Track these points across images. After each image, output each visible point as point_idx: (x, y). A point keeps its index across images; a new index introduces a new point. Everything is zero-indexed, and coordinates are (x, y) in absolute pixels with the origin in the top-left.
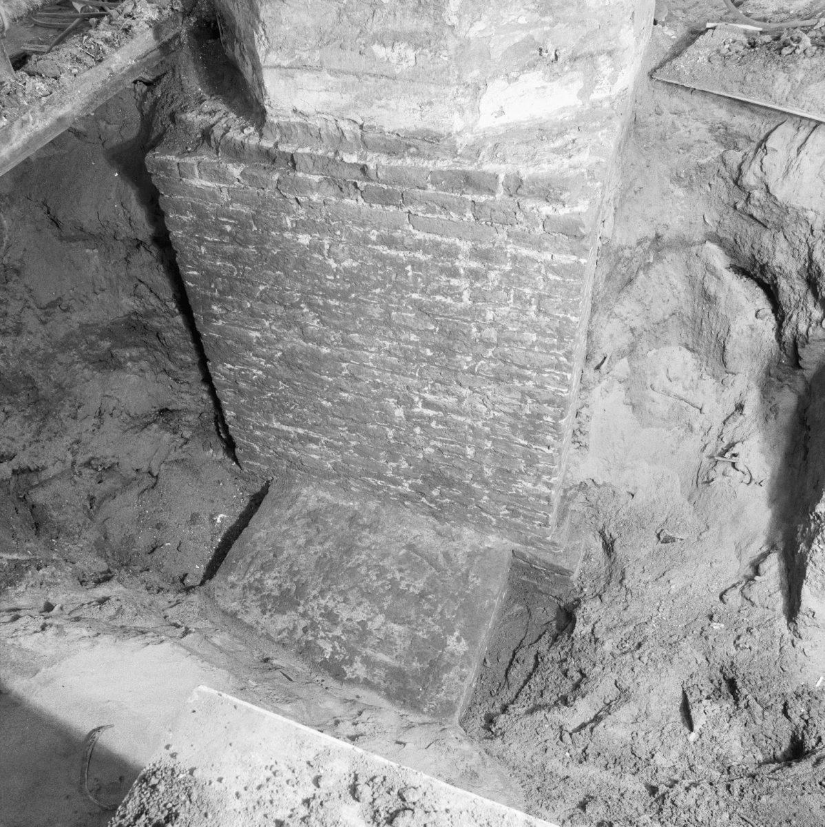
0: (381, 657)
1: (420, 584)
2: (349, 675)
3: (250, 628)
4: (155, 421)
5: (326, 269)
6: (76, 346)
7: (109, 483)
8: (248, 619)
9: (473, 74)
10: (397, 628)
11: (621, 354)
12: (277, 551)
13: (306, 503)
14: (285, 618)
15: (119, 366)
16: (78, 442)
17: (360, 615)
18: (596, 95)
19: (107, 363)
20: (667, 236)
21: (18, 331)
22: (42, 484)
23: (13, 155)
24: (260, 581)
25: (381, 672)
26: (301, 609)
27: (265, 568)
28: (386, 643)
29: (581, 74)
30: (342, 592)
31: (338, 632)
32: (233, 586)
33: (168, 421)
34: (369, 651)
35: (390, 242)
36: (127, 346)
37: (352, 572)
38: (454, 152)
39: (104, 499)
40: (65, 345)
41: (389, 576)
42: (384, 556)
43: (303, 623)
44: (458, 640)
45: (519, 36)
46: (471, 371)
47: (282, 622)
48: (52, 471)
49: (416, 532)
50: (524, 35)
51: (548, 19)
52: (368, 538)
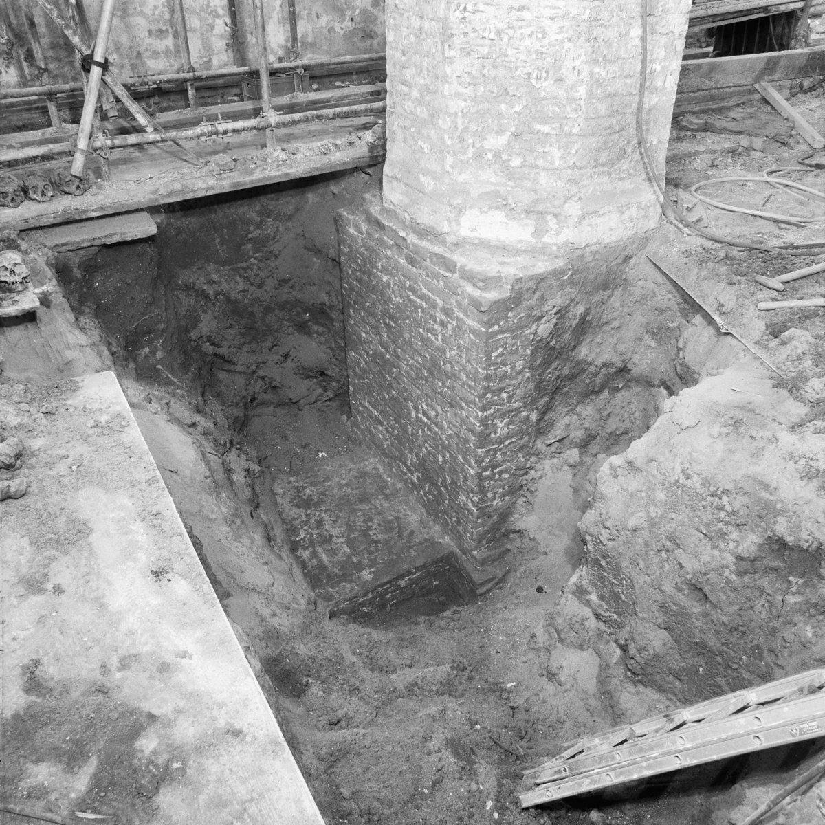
0: (324, 557)
1: (381, 537)
2: (298, 553)
3: (277, 504)
4: (316, 377)
5: (390, 299)
6: (289, 311)
7: (269, 396)
8: (279, 500)
9: (458, 201)
10: (346, 548)
11: (574, 445)
12: (327, 479)
13: (366, 466)
14: (298, 511)
15: (309, 334)
16: (264, 363)
17: (334, 532)
18: (546, 239)
19: (302, 328)
20: (635, 371)
21: (260, 286)
22: (229, 371)
23: (252, 182)
24: (304, 488)
25: (315, 562)
26: (309, 512)
27: (313, 484)
28: (333, 553)
29: (533, 222)
30: (338, 517)
31: (315, 532)
32: (290, 482)
33: (323, 381)
34: (320, 550)
35: (413, 291)
36: (317, 323)
37: (354, 511)
38: (444, 242)
39: (263, 403)
40: (283, 306)
41: (370, 524)
42: (379, 513)
43: (304, 519)
44: (370, 573)
45: (490, 188)
46: (440, 394)
47: (295, 512)
48: (239, 368)
49: (409, 513)
50: (493, 188)
51: (511, 184)
52: (380, 502)
